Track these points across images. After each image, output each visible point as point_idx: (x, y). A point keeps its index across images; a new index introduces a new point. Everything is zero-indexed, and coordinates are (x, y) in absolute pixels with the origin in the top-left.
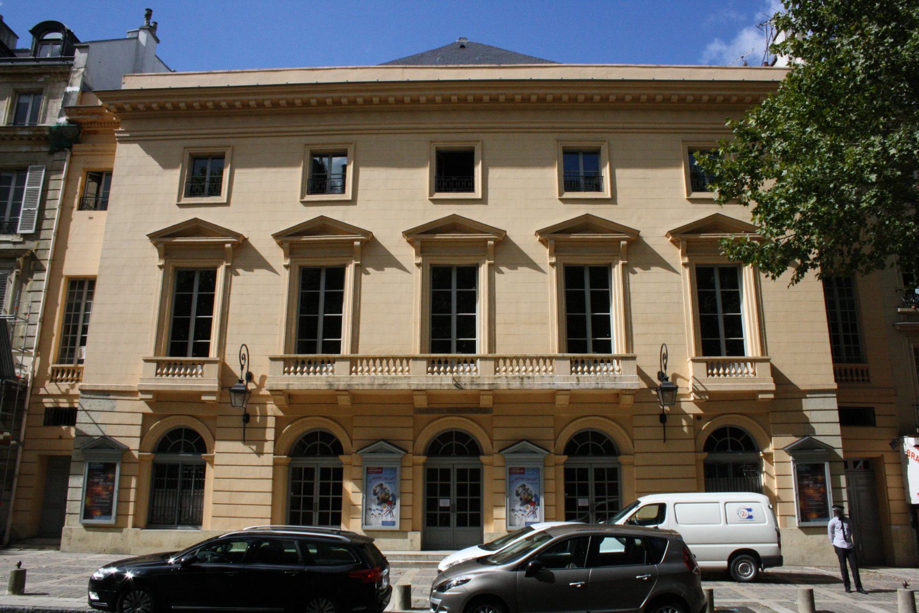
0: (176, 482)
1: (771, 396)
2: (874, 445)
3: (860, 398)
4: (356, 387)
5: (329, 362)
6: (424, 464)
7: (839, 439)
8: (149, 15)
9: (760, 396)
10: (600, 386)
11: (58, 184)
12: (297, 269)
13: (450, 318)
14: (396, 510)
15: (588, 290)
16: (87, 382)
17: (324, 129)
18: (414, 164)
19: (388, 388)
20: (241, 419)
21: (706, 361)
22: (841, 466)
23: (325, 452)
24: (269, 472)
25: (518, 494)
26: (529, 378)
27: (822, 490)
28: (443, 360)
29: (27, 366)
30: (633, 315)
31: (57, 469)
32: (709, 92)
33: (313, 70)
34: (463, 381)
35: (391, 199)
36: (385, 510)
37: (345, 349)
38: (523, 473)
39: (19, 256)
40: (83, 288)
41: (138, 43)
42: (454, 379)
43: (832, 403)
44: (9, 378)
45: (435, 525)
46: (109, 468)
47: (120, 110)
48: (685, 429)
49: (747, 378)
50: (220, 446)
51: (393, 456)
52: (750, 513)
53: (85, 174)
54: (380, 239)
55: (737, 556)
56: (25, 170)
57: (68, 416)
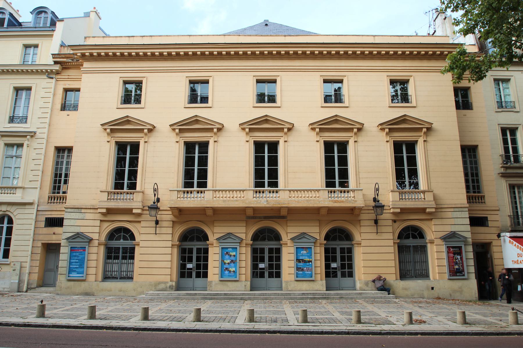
0: (119, 256)
20: (154, 222)
45: (330, 277)
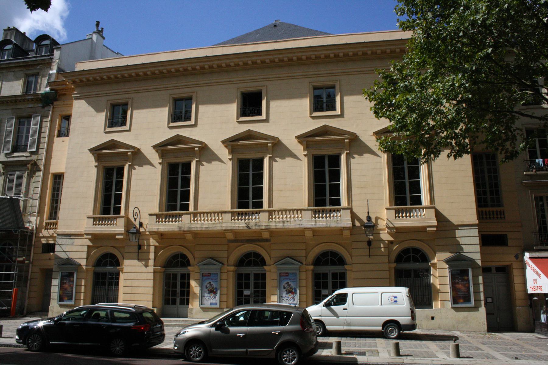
0: (105, 282)
1: (435, 229)
2: (502, 256)
3: (496, 228)
4: (193, 229)
5: (256, 213)
6: (313, 270)
7: (479, 254)
8: (98, 24)
9: (428, 229)
10: (328, 225)
11: (47, 124)
12: (166, 165)
13: (248, 189)
14: (218, 297)
15: (327, 169)
16: (60, 230)
17: (179, 85)
18: (228, 101)
19: (211, 229)
20: (366, 243)
21: (395, 209)
22: (480, 271)
23: (256, 264)
24: (151, 276)
25: (284, 288)
26: (288, 221)
27: (467, 285)
28: (240, 213)
29: (32, 222)
30: (352, 183)
31: (48, 275)
32: (399, 46)
33: (174, 52)
34: (251, 224)
35: (216, 123)
36: (290, 297)
37: (265, 206)
38: (288, 276)
39: (28, 164)
40: (58, 178)
41: (92, 41)
42: (246, 223)
43: (475, 232)
44: (21, 228)
45: (184, 304)
46: (71, 275)
47: (74, 82)
48: (383, 249)
49: (423, 218)
50: (126, 262)
51: (295, 266)
52: (396, 299)
53: (60, 118)
54: (209, 146)
55: (386, 324)
56: (31, 117)
57: (50, 248)
